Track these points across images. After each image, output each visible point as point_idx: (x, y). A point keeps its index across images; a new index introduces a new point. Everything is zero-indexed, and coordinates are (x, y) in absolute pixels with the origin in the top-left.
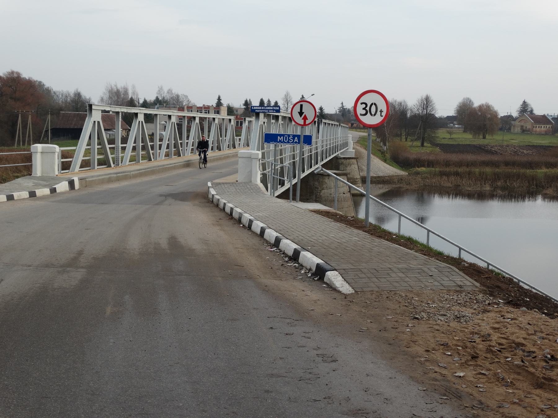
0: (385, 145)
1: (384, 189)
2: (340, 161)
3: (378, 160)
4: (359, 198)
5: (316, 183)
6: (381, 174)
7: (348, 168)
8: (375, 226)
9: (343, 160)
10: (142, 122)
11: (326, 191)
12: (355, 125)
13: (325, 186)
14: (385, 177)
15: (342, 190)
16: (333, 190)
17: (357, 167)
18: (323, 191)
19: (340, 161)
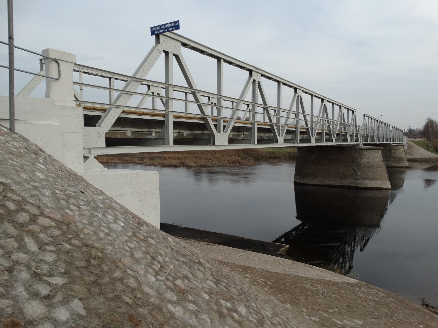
0: (431, 143)
1: (428, 166)
2: (392, 147)
3: (423, 149)
4: (405, 169)
5: (357, 155)
6: (424, 157)
7: (398, 151)
8: (151, 128)
9: (394, 147)
10: (279, 136)
11: (364, 160)
12: (416, 136)
13: (364, 157)
14: (426, 159)
15: (377, 160)
16: (370, 160)
17: (403, 150)
18: (362, 160)
19: (392, 147)
